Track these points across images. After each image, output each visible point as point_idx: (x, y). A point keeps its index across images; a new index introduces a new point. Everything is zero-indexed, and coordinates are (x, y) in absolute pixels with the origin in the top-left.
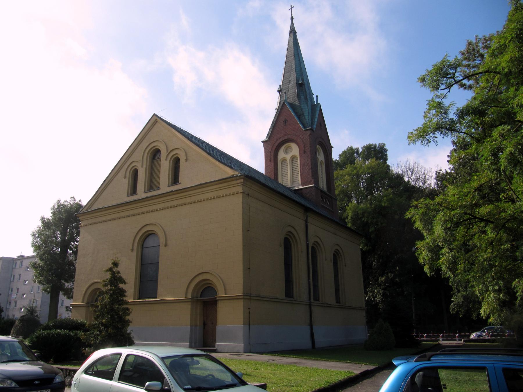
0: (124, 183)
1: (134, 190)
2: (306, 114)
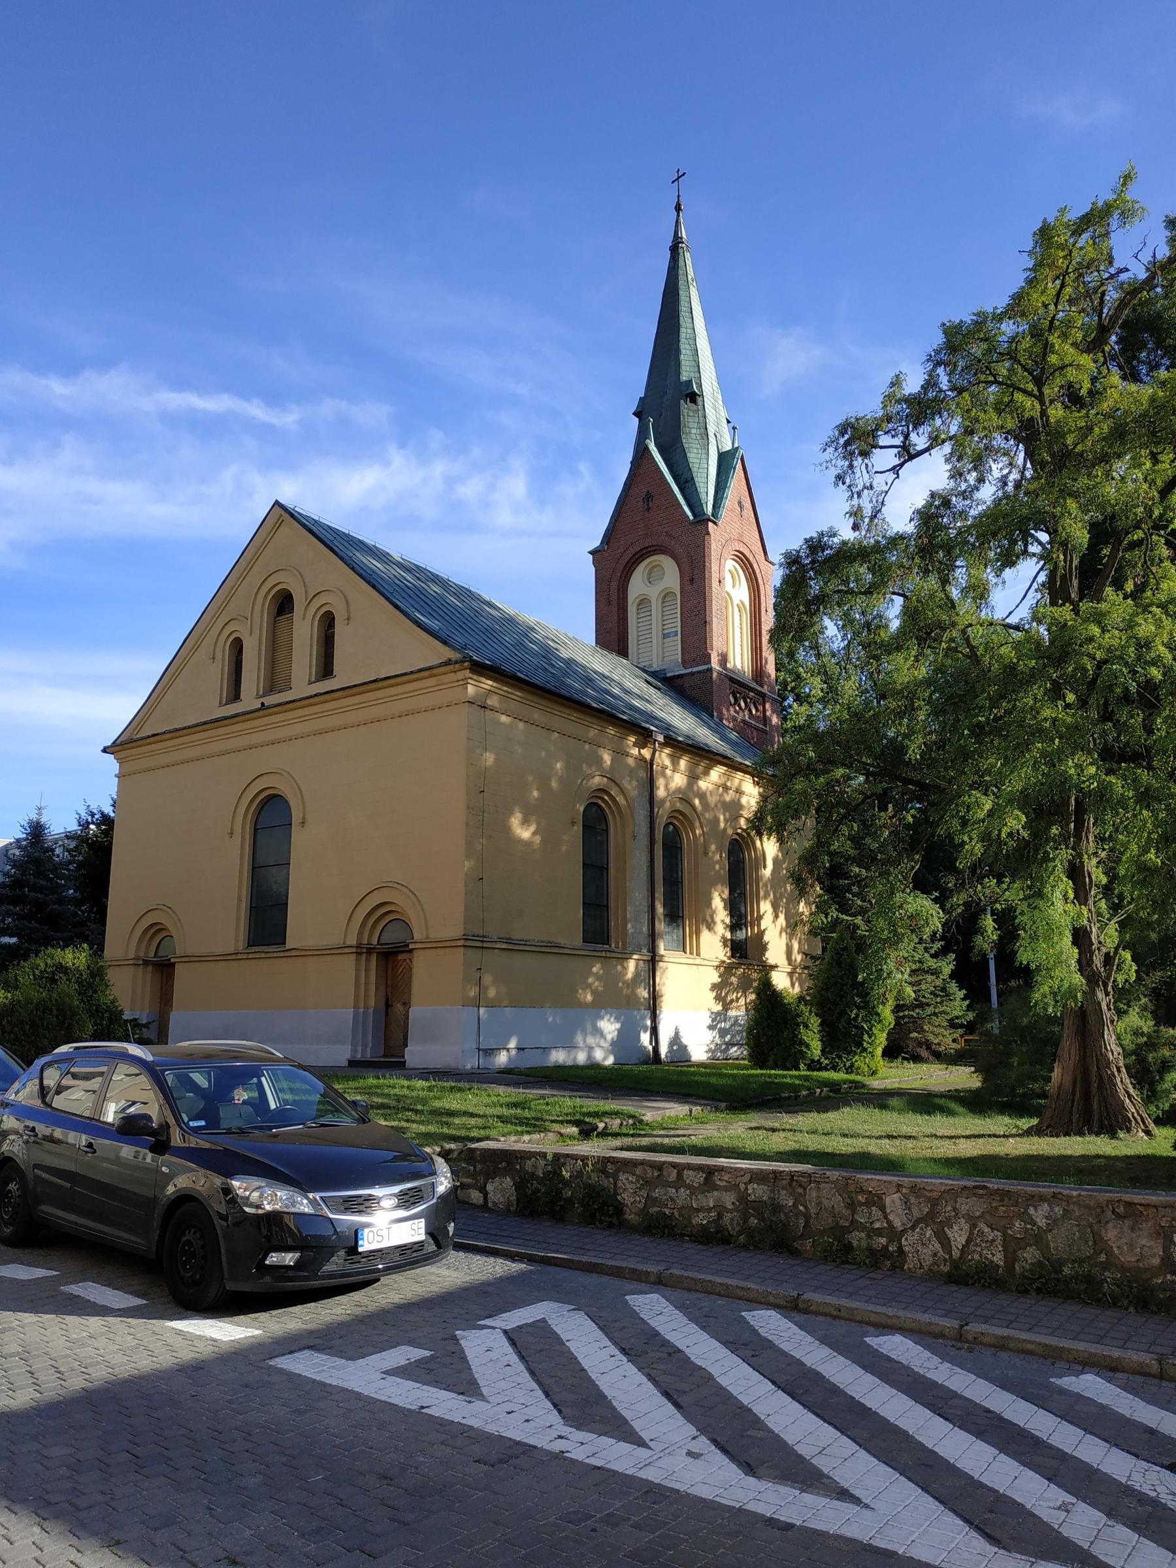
0: (216, 674)
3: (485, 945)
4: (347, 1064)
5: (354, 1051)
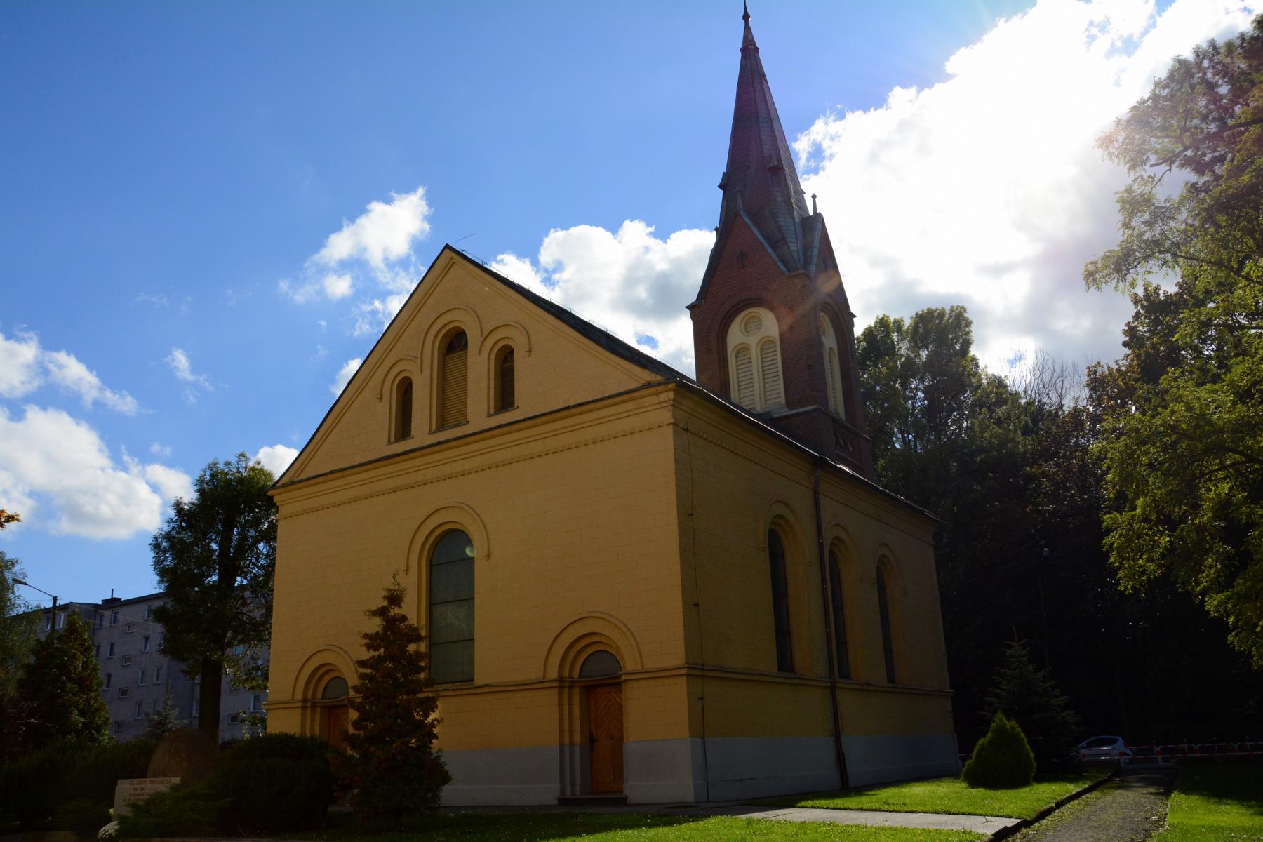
0: (383, 413)
1: (403, 428)
2: (791, 239)
3: (706, 673)
4: (556, 802)
5: (563, 790)
